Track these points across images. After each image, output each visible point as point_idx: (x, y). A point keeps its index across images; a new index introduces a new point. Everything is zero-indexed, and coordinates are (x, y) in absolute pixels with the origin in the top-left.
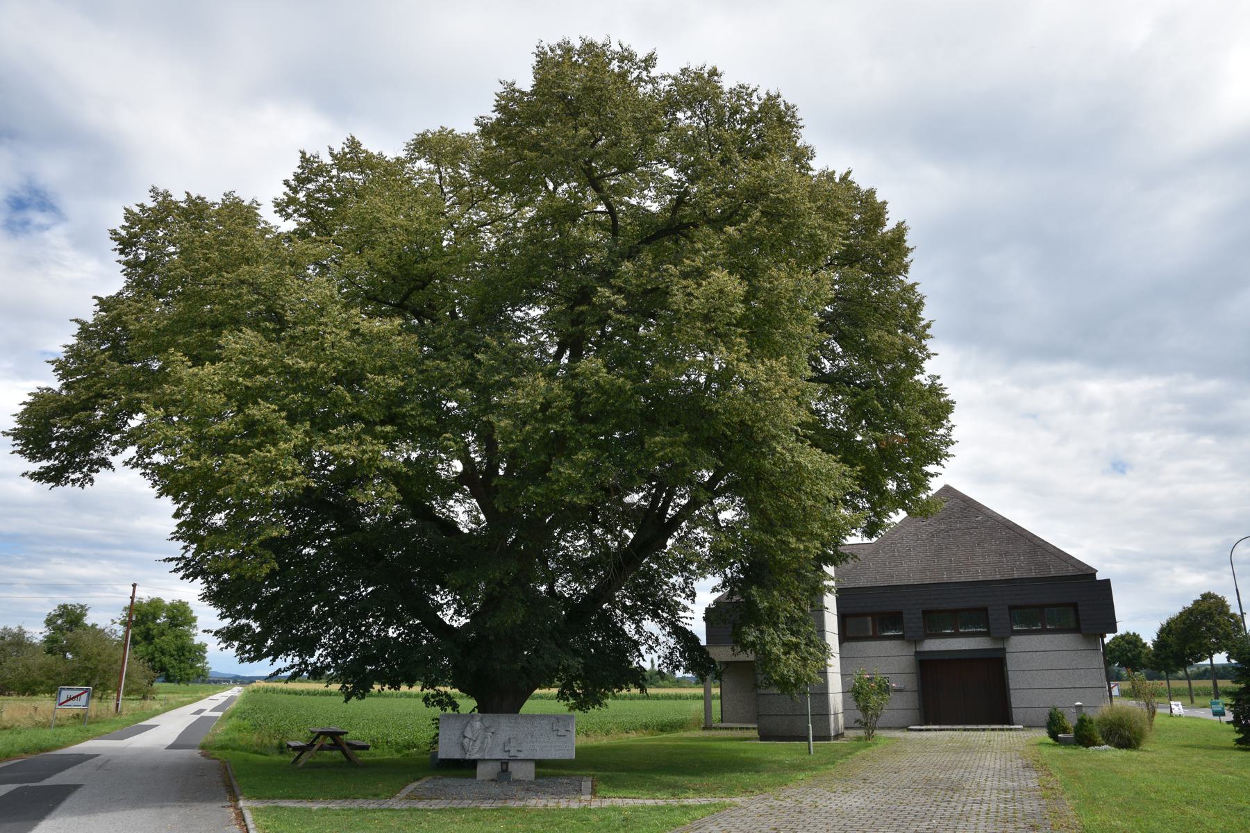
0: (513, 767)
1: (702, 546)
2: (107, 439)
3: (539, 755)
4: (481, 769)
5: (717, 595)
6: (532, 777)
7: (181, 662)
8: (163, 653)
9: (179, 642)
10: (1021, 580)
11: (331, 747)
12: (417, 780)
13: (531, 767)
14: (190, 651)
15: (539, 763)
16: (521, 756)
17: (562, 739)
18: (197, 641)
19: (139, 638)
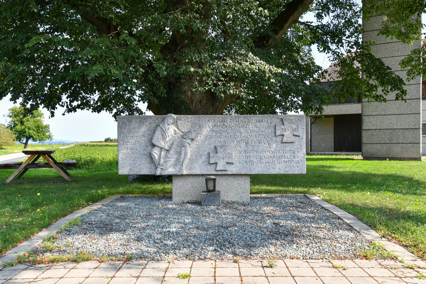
0: (222, 185)
1: (175, 165)
2: (280, 241)
3: (258, 169)
4: (178, 188)
5: (15, 277)
6: (246, 197)
7: (38, 133)
8: (29, 129)
9: (36, 125)
10: (148, 176)
11: (47, 165)
12: (94, 200)
13: (246, 183)
14: (42, 128)
15: (256, 179)
16: (232, 170)
17: (289, 147)
18: (45, 123)
19: (17, 123)
